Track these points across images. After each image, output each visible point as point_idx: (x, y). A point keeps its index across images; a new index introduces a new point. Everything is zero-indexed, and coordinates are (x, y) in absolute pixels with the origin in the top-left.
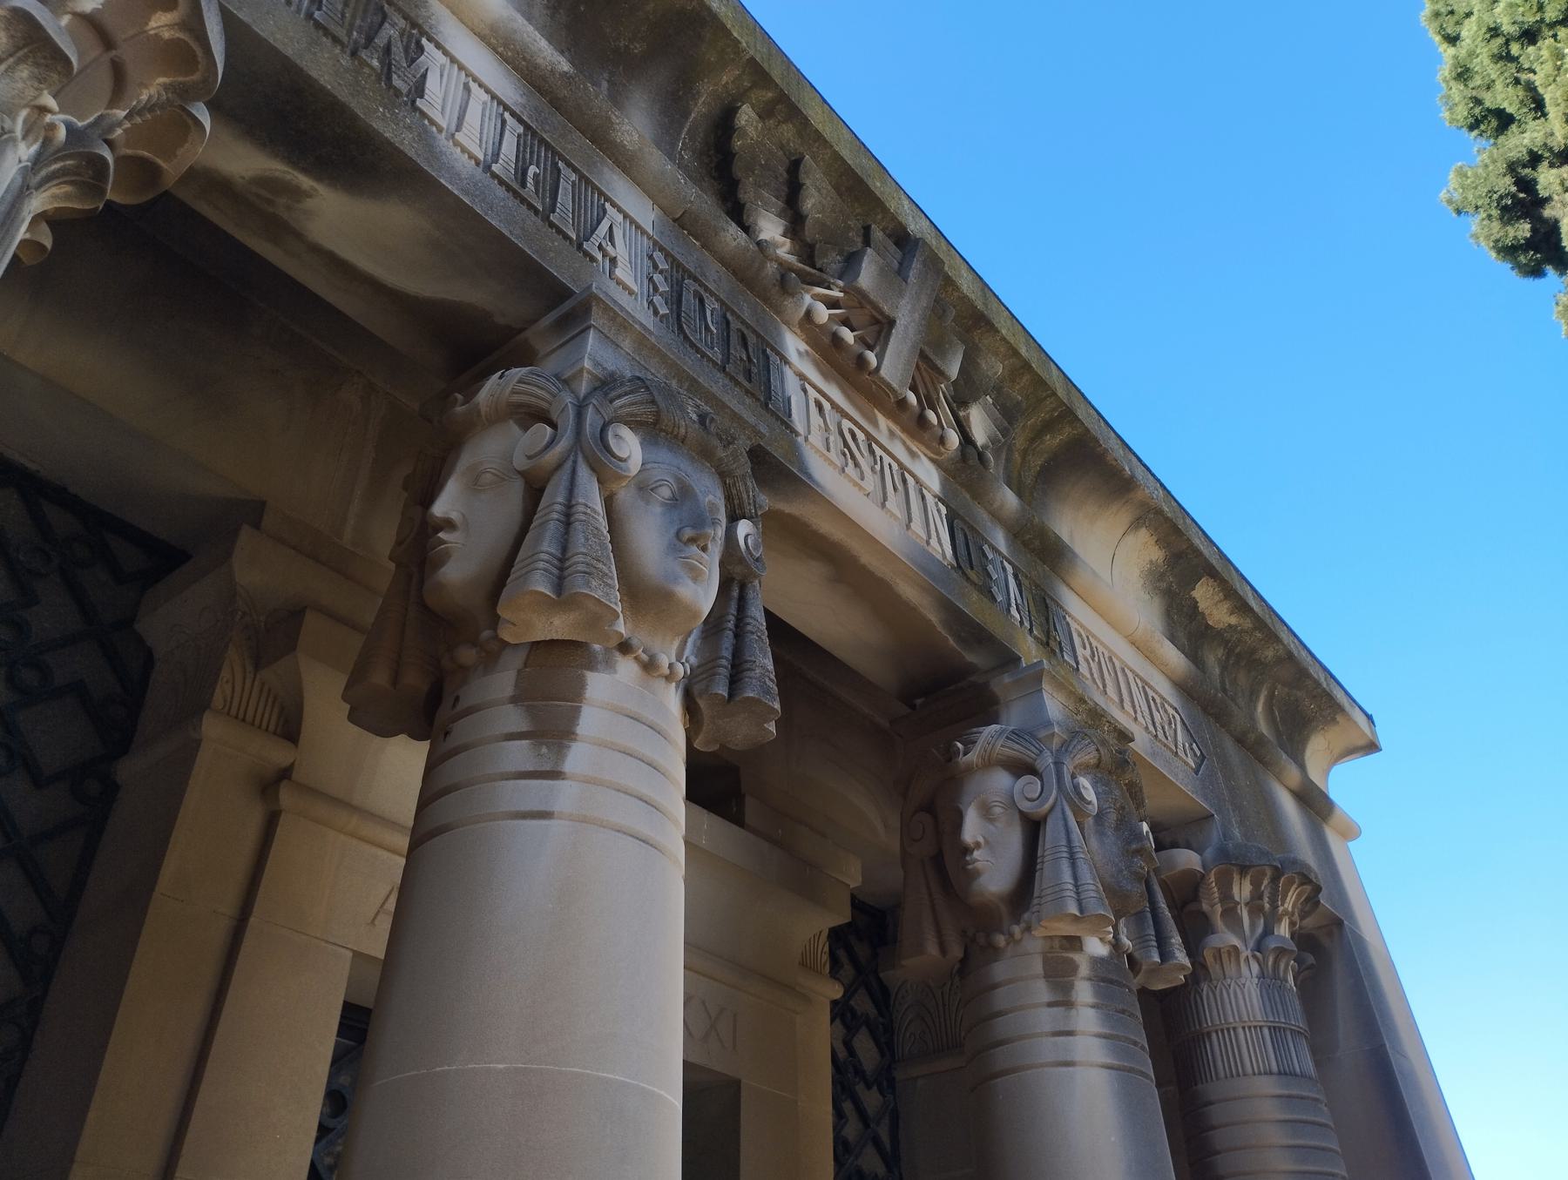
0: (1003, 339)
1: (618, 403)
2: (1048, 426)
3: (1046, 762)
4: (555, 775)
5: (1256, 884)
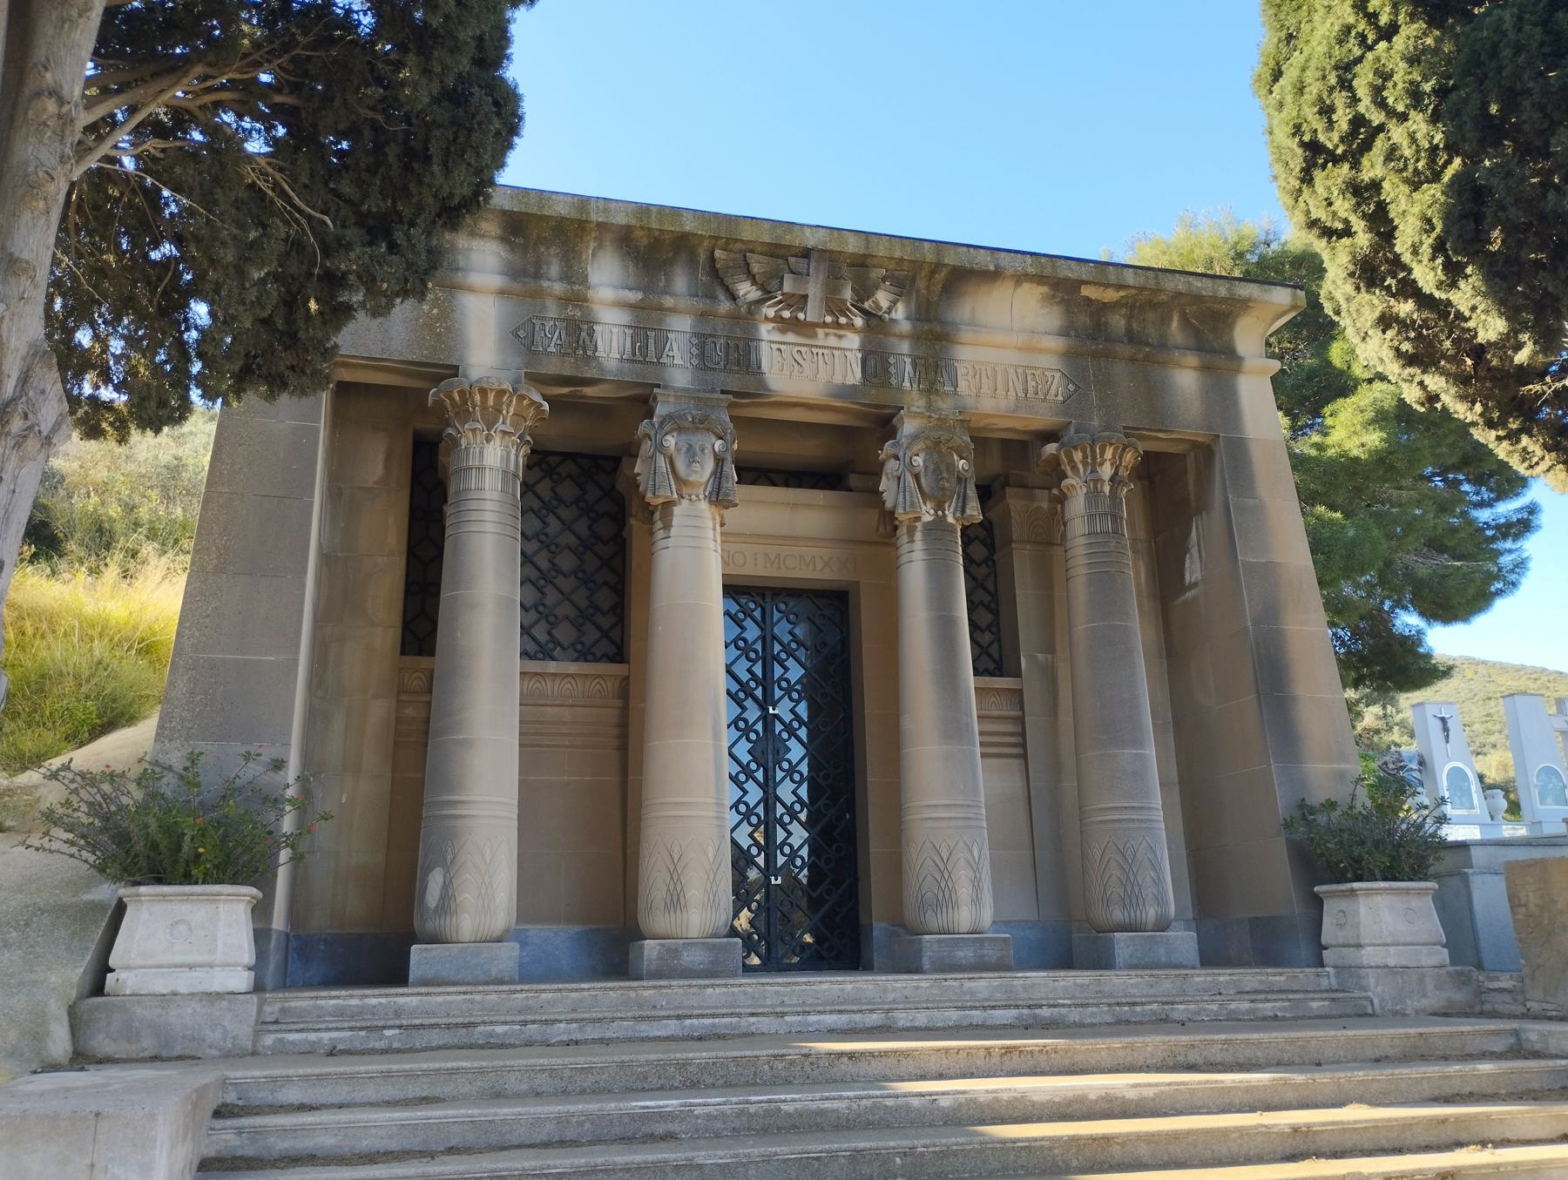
2: (933, 273)
3: (901, 455)
5: (1084, 452)
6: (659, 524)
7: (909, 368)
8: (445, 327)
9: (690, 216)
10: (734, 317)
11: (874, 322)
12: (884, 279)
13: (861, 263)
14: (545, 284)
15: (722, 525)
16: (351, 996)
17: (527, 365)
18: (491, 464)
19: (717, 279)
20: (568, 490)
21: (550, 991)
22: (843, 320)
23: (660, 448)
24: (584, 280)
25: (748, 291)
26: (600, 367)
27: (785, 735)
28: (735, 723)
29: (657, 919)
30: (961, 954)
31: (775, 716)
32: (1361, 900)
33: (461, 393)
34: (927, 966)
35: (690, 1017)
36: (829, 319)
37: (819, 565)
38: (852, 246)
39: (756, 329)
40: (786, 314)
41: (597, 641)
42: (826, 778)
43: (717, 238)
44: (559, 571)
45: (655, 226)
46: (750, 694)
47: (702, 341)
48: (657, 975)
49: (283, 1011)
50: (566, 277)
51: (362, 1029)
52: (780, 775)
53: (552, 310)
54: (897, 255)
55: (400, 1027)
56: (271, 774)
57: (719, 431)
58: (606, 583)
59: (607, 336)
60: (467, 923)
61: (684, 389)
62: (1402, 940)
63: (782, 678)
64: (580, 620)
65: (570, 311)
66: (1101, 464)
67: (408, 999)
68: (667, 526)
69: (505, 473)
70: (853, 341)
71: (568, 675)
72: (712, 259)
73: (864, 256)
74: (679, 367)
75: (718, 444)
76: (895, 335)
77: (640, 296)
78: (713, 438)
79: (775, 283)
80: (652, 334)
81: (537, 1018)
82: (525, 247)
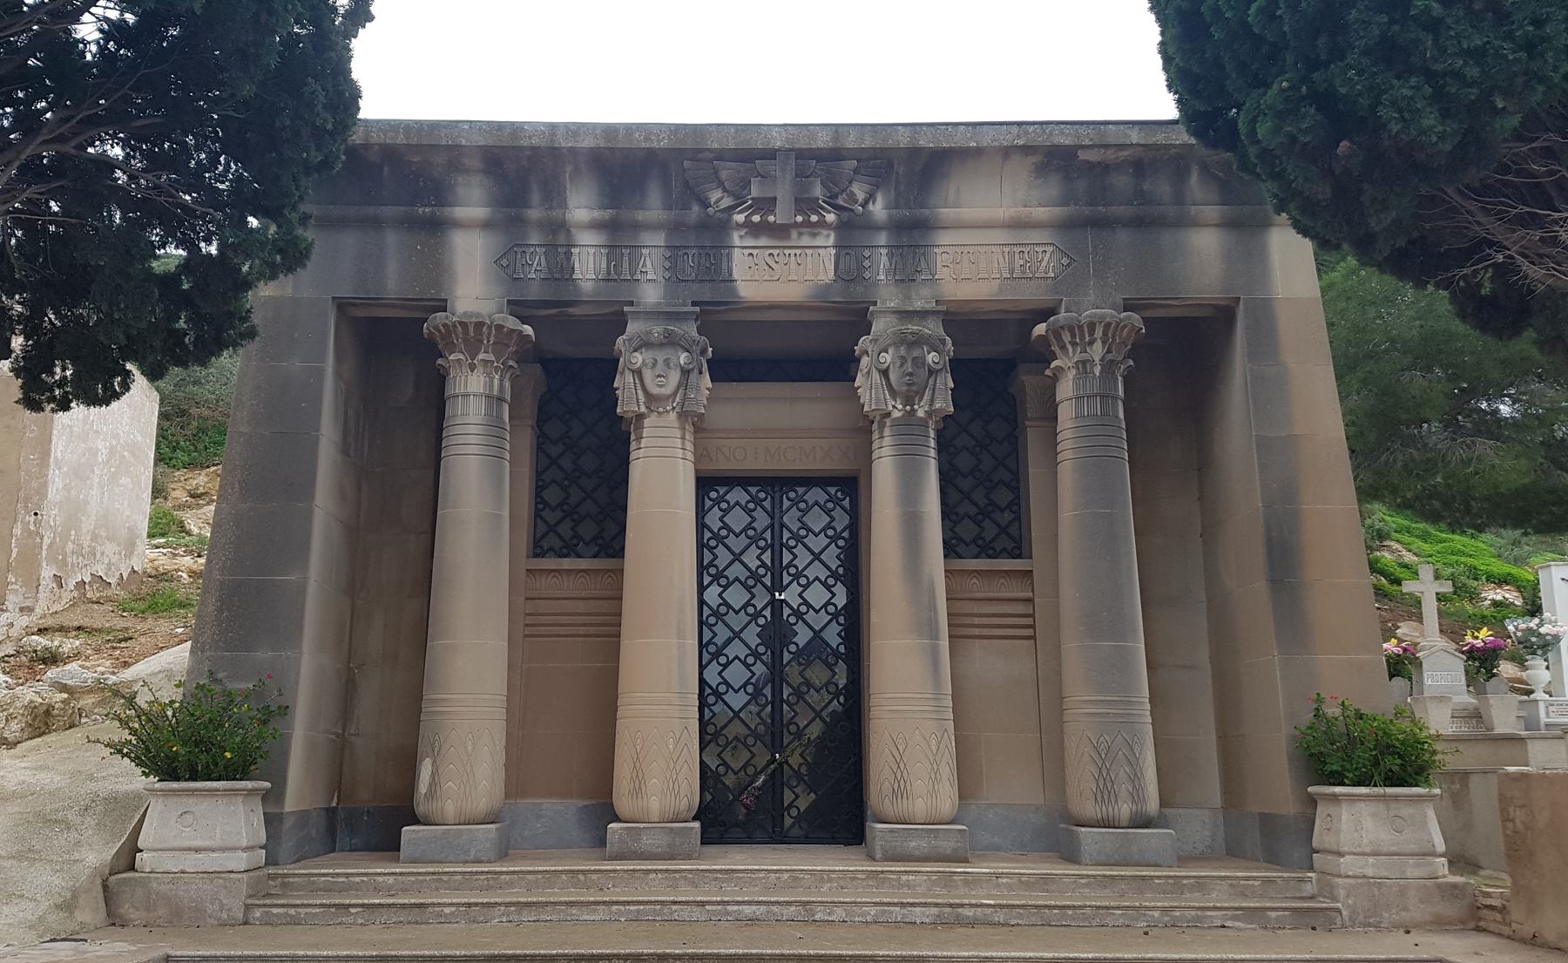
7: (884, 259)
8: (435, 266)
22: (814, 218)
27: (792, 620)
30: (913, 844)
32: (1344, 805)
34: (878, 856)
36: (799, 219)
39: (729, 236)
40: (756, 218)
59: (584, 256)
62: (1385, 850)
66: (1091, 343)
80: (626, 251)
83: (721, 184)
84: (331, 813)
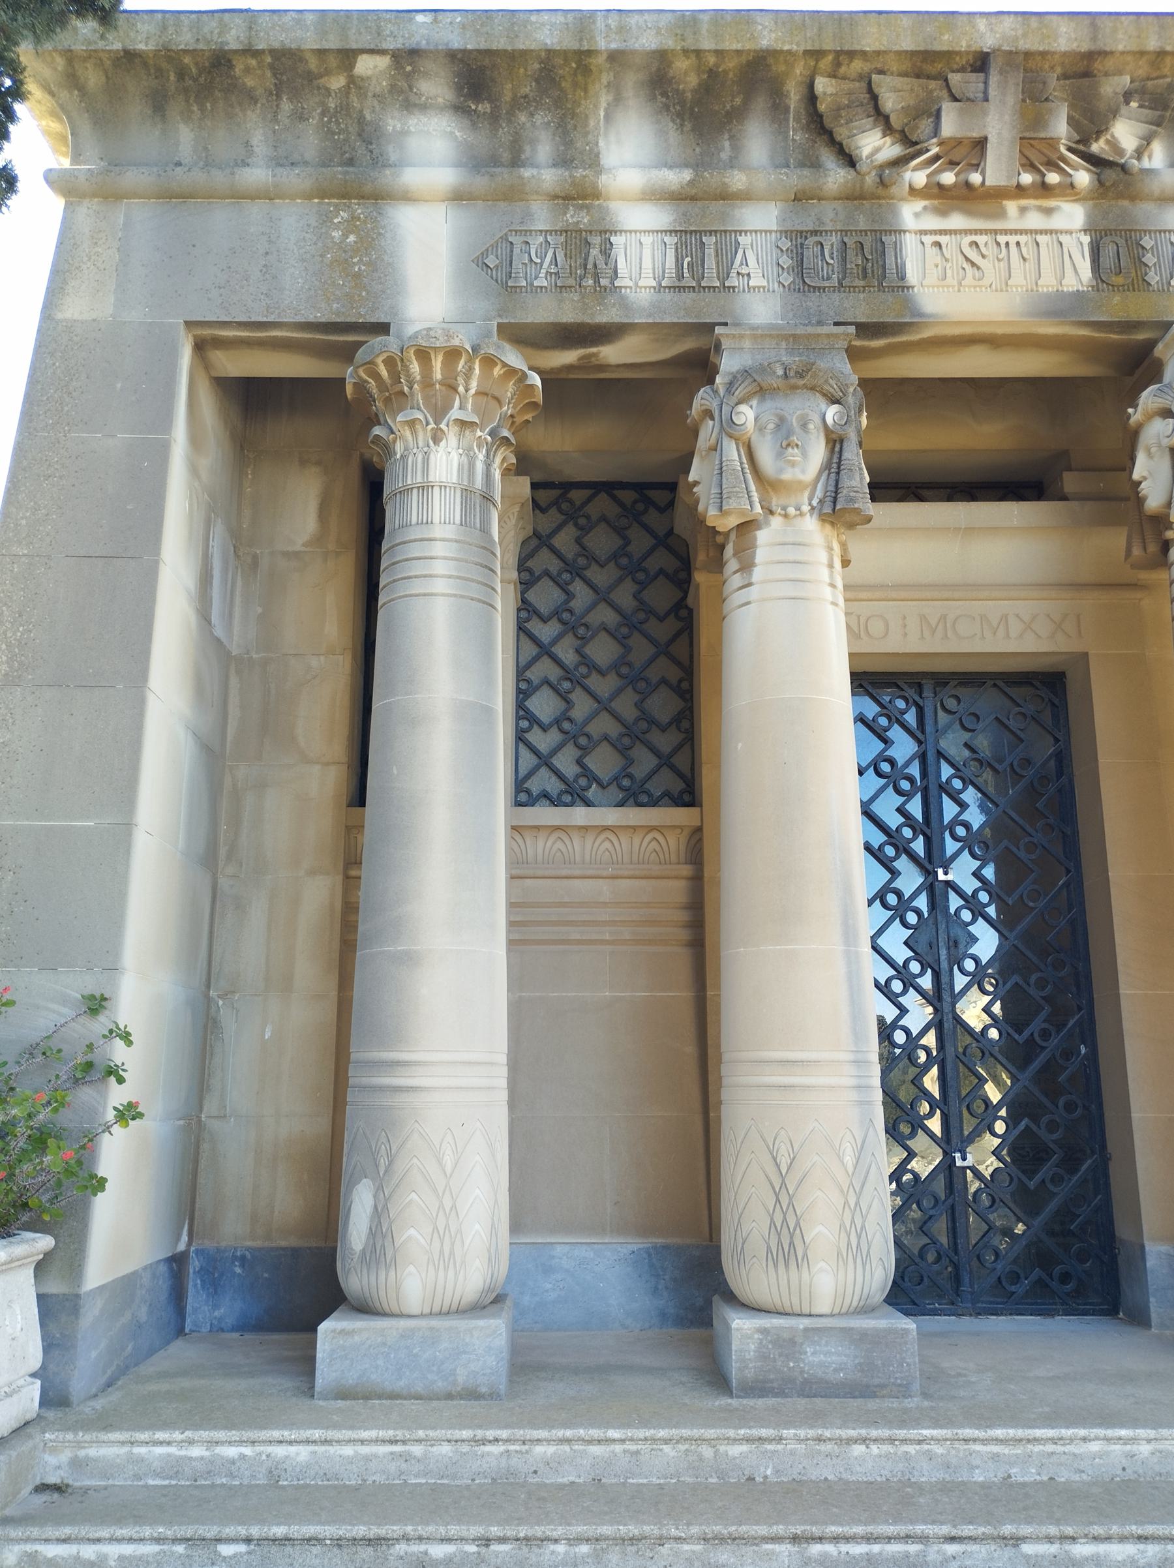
0: (1123, 53)
1: (737, 393)
4: (750, 585)
6: (732, 565)
8: (365, 259)
9: (767, 21)
10: (854, 196)
11: (1110, 175)
12: (1128, 96)
13: (1083, 70)
14: (527, 173)
15: (846, 563)
16: (191, 1442)
17: (501, 312)
18: (451, 484)
19: (823, 132)
20: (602, 541)
21: (549, 1441)
22: (1053, 178)
23: (729, 428)
24: (594, 162)
25: (874, 145)
26: (624, 304)
27: (966, 915)
28: (880, 897)
29: (751, 1274)
31: (948, 884)
33: (390, 362)
35: (821, 1539)
36: (1027, 178)
37: (1015, 627)
38: (1066, 41)
39: (895, 212)
41: (654, 772)
42: (1042, 984)
43: (816, 54)
44: (592, 667)
45: (707, 44)
46: (904, 849)
47: (799, 244)
48: (757, 1389)
49: (77, 1464)
50: (563, 161)
51: (176, 1540)
52: (960, 981)
53: (541, 216)
54: (1152, 44)
55: (248, 1540)
56: (83, 1019)
57: (834, 388)
58: (664, 681)
59: (633, 251)
60: (413, 1282)
61: (772, 327)
63: (956, 821)
64: (626, 741)
65: (571, 217)
67: (293, 1449)
68: (747, 566)
69: (467, 492)
70: (1072, 216)
71: (606, 828)
72: (811, 98)
73: (1091, 56)
74: (760, 292)
75: (832, 413)
76: (1149, 198)
77: (687, 175)
78: (822, 403)
79: (926, 125)
80: (710, 241)
81: (510, 1532)
82: (494, 118)
83: (882, 119)
84: (177, 1262)
